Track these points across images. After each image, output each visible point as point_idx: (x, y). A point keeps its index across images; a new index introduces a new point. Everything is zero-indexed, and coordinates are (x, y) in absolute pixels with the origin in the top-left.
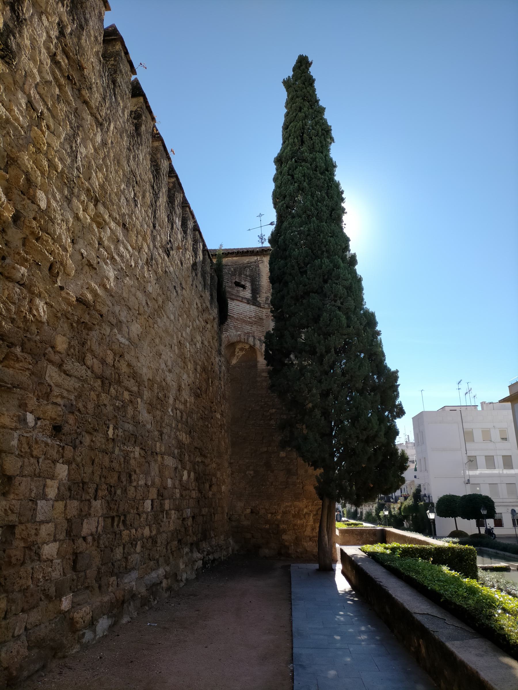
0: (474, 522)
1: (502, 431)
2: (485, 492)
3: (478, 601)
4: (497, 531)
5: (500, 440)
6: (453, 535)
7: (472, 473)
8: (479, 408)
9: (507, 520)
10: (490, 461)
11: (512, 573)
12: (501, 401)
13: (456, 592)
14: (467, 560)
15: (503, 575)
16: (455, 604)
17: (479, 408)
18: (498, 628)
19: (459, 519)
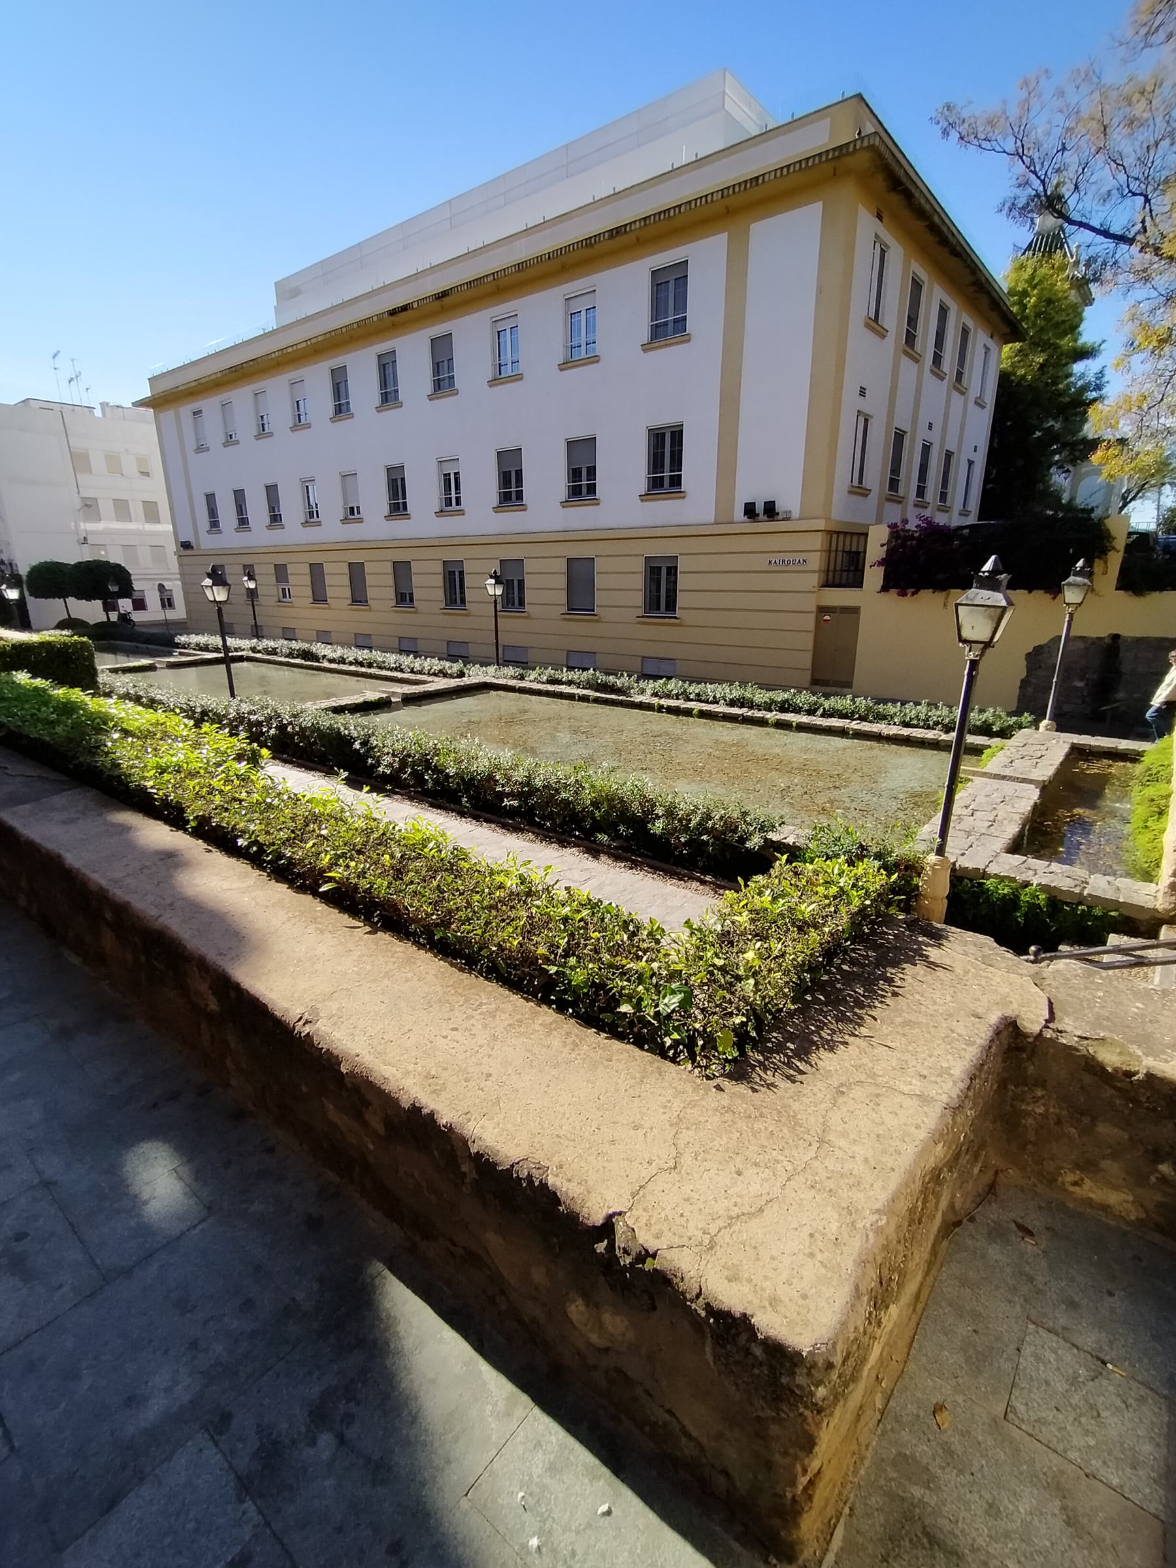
0: (98, 603)
1: (141, 460)
2: (114, 557)
3: (77, 725)
4: (137, 617)
5: (138, 474)
6: (61, 625)
7: (90, 526)
8: (98, 413)
9: (153, 600)
10: (122, 509)
11: (158, 672)
12: (134, 404)
13: (33, 715)
14: (78, 659)
15: (145, 677)
16: (28, 737)
17: (98, 413)
18: (109, 766)
19: (71, 600)
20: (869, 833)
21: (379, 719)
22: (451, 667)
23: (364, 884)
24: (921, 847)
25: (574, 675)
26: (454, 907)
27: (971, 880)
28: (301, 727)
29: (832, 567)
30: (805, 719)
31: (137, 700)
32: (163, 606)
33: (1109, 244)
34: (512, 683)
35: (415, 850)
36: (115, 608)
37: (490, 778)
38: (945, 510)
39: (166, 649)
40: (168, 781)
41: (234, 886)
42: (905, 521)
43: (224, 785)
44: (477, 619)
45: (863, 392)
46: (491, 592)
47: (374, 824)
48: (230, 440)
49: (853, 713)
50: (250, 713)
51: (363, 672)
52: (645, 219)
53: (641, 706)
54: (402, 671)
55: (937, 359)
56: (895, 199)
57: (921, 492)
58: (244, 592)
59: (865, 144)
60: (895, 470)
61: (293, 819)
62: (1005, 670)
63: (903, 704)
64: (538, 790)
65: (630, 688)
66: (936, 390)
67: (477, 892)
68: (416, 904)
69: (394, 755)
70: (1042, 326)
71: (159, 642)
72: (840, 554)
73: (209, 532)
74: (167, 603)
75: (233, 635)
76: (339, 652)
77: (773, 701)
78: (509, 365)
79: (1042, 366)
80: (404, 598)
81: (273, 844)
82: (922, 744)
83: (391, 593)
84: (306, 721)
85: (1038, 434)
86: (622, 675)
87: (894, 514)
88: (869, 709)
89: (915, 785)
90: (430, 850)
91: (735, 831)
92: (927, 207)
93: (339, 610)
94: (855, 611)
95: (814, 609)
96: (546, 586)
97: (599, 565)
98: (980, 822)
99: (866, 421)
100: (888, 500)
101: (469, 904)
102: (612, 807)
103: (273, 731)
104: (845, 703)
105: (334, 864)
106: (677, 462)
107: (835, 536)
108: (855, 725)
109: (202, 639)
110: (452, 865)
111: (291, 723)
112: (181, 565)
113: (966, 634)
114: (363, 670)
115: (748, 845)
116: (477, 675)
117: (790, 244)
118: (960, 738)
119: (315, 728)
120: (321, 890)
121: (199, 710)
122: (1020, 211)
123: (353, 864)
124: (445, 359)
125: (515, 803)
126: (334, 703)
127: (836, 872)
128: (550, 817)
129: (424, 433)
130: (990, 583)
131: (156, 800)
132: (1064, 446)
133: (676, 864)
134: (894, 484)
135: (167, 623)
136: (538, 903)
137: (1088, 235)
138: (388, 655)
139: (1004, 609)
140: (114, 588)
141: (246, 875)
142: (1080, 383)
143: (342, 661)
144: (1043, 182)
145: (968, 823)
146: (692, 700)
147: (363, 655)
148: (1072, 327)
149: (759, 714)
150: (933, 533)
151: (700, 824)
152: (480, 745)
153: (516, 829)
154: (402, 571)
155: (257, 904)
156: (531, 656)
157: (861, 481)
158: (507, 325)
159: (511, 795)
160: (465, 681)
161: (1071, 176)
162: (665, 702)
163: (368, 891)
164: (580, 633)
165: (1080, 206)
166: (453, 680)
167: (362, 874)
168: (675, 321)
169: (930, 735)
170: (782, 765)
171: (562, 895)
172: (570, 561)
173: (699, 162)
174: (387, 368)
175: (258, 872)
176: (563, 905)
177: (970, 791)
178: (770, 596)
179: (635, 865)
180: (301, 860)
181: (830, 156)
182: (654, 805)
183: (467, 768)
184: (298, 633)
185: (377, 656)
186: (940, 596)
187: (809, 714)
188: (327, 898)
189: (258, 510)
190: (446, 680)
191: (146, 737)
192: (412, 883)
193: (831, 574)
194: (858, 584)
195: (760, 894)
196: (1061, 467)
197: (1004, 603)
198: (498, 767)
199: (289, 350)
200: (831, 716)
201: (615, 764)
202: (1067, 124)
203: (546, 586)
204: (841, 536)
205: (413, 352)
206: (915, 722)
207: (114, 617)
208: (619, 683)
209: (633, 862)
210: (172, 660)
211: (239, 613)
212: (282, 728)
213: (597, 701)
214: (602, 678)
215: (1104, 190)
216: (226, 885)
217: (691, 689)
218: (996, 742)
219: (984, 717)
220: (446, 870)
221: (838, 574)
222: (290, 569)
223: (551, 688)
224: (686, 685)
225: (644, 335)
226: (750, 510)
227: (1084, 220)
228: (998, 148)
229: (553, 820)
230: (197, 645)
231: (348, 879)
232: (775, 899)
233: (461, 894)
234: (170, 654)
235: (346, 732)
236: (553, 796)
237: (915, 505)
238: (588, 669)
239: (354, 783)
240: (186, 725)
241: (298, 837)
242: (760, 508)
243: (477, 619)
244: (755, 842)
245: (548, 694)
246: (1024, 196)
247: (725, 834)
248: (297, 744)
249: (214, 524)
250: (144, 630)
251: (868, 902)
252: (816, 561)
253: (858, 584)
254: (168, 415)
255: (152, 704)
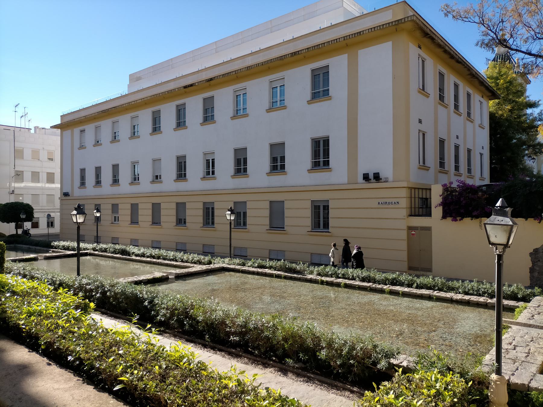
0: (13, 225)
2: (27, 200)
4: (33, 232)
7: (17, 185)
8: (32, 131)
9: (43, 223)
10: (35, 177)
11: (39, 262)
12: (51, 127)
17: (32, 131)
20: (452, 358)
21: (162, 288)
22: (204, 259)
23: (141, 385)
24: (486, 369)
25: (272, 263)
26: (196, 400)
27: (521, 392)
28: (115, 293)
29: (413, 206)
30: (406, 290)
31: (24, 276)
32: (48, 226)
33: (533, 59)
34: (238, 267)
35: (175, 363)
36: (21, 227)
37: (223, 323)
38: (472, 177)
39: (45, 249)
40: (33, 321)
41: (62, 387)
42: (451, 183)
43: (66, 323)
44: (220, 233)
45: (420, 121)
46: (228, 218)
47: (151, 347)
48: (97, 143)
49: (434, 286)
50: (87, 284)
51: (155, 261)
52: (308, 48)
53: (311, 281)
54: (176, 261)
55: (456, 107)
56: (426, 41)
57: (457, 168)
58: (94, 218)
59: (410, 19)
60: (442, 158)
61: (103, 344)
62: (519, 264)
63: (463, 281)
64: (251, 330)
65: (304, 271)
66: (458, 121)
67: (211, 391)
68: (172, 398)
69: (167, 309)
70: (507, 91)
71: (43, 245)
72: (417, 199)
73: (79, 188)
74: (51, 224)
75: (84, 241)
76: (142, 250)
77: (387, 279)
78: (242, 110)
79: (510, 111)
80: (181, 221)
81: (89, 359)
82: (478, 305)
83: (174, 219)
84: (118, 289)
85: (515, 141)
86: (300, 263)
87: (444, 179)
88: (443, 284)
89: (476, 330)
90: (183, 363)
91: (370, 358)
92: (442, 43)
93: (145, 229)
94: (429, 229)
95: (406, 228)
96: (258, 216)
97: (287, 205)
98: (520, 353)
99: (424, 135)
100: (440, 172)
101: (205, 398)
102: (295, 341)
103: (98, 295)
104: (428, 280)
105: (124, 372)
106: (327, 153)
107: (413, 190)
108: (436, 293)
109: (66, 244)
110: (196, 373)
111: (109, 290)
112: (61, 204)
113: (493, 240)
114: (154, 260)
115: (379, 366)
116: (218, 263)
117: (378, 63)
118: (499, 301)
119: (123, 293)
120: (115, 389)
121: (58, 282)
122: (488, 45)
123: (136, 372)
124: (210, 107)
125: (237, 339)
126: (136, 278)
127: (433, 379)
128: (258, 348)
129: (196, 141)
130: (501, 212)
131: (23, 332)
132: (529, 146)
133: (335, 379)
134: (442, 164)
135: (48, 235)
136: (249, 398)
137: (521, 55)
138: (169, 252)
139: (512, 227)
140: (23, 216)
141: (70, 380)
142: (531, 117)
143: (143, 255)
144: (495, 34)
145: (512, 354)
146: (340, 278)
147: (155, 252)
148: (521, 92)
149: (380, 286)
150: (467, 189)
151: (348, 353)
152: (218, 303)
153: (236, 356)
154: (181, 207)
155: (73, 399)
156: (249, 253)
157: (424, 163)
158: (241, 93)
159: (235, 334)
160: (212, 266)
161: (508, 31)
162: (324, 279)
163: (144, 390)
164: (277, 240)
165: (515, 43)
166: (205, 266)
167: (141, 379)
168: (323, 91)
169: (482, 299)
170: (396, 318)
171: (263, 393)
172: (271, 202)
173: (332, 27)
174: (181, 112)
175: (77, 378)
176: (264, 400)
177: (511, 334)
178: (383, 225)
179: (309, 380)
180: (104, 370)
181: (394, 24)
182: (320, 341)
183: (209, 317)
184: (120, 241)
185: (163, 252)
186: (476, 222)
187: (409, 287)
188: (117, 395)
189: (107, 176)
190: (201, 266)
191: (25, 296)
192: (171, 384)
193: (413, 209)
194: (429, 214)
195: (387, 394)
196: (530, 157)
197: (511, 223)
198: (227, 316)
199: (133, 103)
200: (422, 288)
201: (296, 315)
202: (502, 12)
203: (258, 216)
204: (417, 190)
205: (194, 106)
206: (471, 292)
207: (20, 231)
208: (298, 268)
209: (309, 378)
210: (48, 255)
211: (89, 230)
212: (104, 293)
213: (286, 278)
214: (288, 265)
215: (525, 37)
216: (56, 386)
217: (339, 271)
218: (521, 304)
219: (511, 289)
220: (192, 376)
221: (417, 209)
222: (120, 206)
223: (260, 270)
224: (336, 269)
225: (309, 97)
226: (366, 177)
227: (518, 48)
228: (471, 21)
229: (259, 349)
230: (63, 246)
231: (132, 382)
232: (397, 397)
233: (200, 392)
234: (47, 252)
235: (141, 296)
236: (260, 334)
237: (455, 175)
238: (281, 260)
239: (142, 324)
240: (49, 289)
241: (105, 354)
242: (371, 176)
243: (220, 233)
244: (382, 365)
245: (258, 274)
246: (487, 39)
247: (364, 359)
248: (111, 303)
249: (83, 184)
250: (35, 239)
251: (456, 400)
252: (404, 203)
253: (429, 214)
254: (68, 133)
255: (32, 278)
